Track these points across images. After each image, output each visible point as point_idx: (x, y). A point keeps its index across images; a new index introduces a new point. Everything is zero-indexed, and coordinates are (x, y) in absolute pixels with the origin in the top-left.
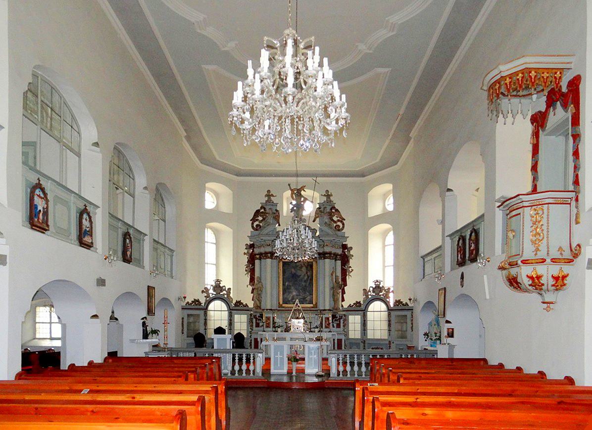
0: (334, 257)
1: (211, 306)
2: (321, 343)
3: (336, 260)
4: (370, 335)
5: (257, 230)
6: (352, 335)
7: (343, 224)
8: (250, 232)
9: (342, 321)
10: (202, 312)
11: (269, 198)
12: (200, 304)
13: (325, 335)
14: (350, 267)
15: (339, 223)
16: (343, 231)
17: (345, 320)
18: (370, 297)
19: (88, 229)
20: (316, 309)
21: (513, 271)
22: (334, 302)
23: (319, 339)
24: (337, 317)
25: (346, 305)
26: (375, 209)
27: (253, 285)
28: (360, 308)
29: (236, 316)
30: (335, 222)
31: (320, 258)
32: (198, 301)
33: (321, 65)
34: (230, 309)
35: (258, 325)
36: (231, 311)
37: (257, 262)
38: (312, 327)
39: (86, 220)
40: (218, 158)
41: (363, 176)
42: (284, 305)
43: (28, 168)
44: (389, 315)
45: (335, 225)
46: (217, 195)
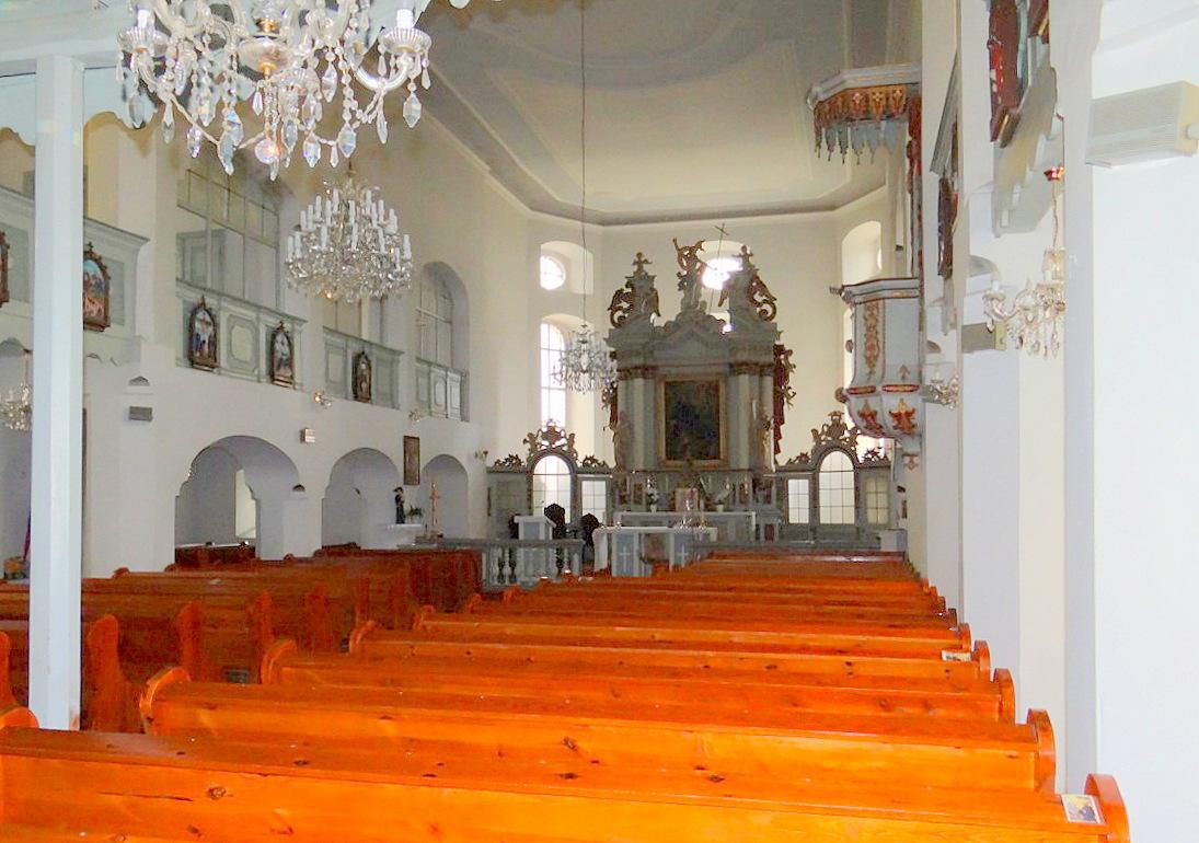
0: (760, 370)
1: (541, 467)
3: (761, 376)
4: (824, 519)
7: (774, 308)
8: (607, 332)
9: (774, 489)
10: (523, 478)
11: (640, 269)
15: (766, 307)
16: (774, 321)
19: (285, 358)
21: (873, 403)
25: (782, 460)
28: (808, 466)
29: (585, 483)
30: (759, 305)
33: (386, 217)
39: (283, 344)
40: (558, 199)
41: (833, 207)
45: (758, 309)
46: (566, 262)
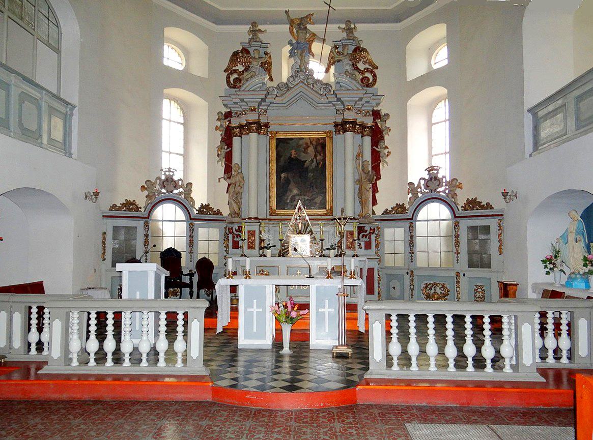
2: (342, 282)
5: (235, 87)
6: (389, 261)
7: (375, 76)
9: (373, 236)
10: (140, 224)
12: (137, 209)
13: (352, 264)
14: (386, 148)
15: (368, 75)
16: (375, 86)
17: (378, 236)
18: (420, 195)
20: (330, 217)
22: (362, 205)
23: (338, 272)
24: (366, 231)
25: (379, 210)
26: (416, 69)
27: (229, 178)
31: (337, 132)
32: (133, 203)
34: (191, 219)
35: (236, 245)
36: (192, 221)
37: (236, 141)
38: (324, 248)
42: (278, 211)
43: (21, 79)
44: (456, 225)
45: (361, 77)
46: (186, 52)
